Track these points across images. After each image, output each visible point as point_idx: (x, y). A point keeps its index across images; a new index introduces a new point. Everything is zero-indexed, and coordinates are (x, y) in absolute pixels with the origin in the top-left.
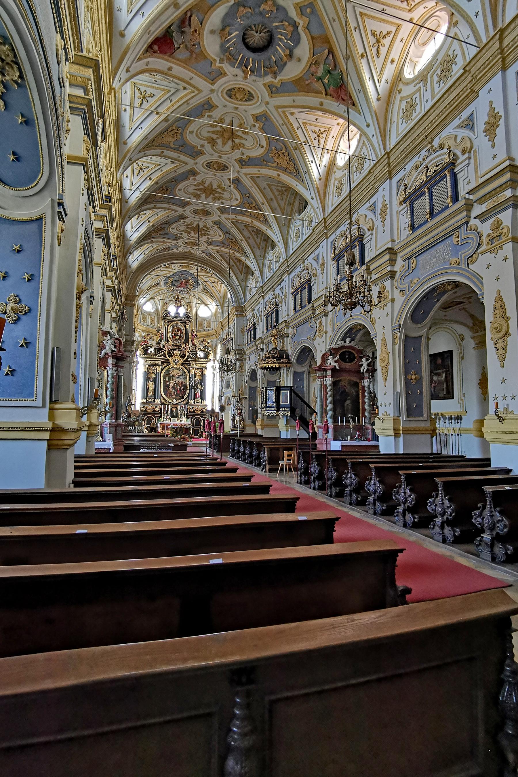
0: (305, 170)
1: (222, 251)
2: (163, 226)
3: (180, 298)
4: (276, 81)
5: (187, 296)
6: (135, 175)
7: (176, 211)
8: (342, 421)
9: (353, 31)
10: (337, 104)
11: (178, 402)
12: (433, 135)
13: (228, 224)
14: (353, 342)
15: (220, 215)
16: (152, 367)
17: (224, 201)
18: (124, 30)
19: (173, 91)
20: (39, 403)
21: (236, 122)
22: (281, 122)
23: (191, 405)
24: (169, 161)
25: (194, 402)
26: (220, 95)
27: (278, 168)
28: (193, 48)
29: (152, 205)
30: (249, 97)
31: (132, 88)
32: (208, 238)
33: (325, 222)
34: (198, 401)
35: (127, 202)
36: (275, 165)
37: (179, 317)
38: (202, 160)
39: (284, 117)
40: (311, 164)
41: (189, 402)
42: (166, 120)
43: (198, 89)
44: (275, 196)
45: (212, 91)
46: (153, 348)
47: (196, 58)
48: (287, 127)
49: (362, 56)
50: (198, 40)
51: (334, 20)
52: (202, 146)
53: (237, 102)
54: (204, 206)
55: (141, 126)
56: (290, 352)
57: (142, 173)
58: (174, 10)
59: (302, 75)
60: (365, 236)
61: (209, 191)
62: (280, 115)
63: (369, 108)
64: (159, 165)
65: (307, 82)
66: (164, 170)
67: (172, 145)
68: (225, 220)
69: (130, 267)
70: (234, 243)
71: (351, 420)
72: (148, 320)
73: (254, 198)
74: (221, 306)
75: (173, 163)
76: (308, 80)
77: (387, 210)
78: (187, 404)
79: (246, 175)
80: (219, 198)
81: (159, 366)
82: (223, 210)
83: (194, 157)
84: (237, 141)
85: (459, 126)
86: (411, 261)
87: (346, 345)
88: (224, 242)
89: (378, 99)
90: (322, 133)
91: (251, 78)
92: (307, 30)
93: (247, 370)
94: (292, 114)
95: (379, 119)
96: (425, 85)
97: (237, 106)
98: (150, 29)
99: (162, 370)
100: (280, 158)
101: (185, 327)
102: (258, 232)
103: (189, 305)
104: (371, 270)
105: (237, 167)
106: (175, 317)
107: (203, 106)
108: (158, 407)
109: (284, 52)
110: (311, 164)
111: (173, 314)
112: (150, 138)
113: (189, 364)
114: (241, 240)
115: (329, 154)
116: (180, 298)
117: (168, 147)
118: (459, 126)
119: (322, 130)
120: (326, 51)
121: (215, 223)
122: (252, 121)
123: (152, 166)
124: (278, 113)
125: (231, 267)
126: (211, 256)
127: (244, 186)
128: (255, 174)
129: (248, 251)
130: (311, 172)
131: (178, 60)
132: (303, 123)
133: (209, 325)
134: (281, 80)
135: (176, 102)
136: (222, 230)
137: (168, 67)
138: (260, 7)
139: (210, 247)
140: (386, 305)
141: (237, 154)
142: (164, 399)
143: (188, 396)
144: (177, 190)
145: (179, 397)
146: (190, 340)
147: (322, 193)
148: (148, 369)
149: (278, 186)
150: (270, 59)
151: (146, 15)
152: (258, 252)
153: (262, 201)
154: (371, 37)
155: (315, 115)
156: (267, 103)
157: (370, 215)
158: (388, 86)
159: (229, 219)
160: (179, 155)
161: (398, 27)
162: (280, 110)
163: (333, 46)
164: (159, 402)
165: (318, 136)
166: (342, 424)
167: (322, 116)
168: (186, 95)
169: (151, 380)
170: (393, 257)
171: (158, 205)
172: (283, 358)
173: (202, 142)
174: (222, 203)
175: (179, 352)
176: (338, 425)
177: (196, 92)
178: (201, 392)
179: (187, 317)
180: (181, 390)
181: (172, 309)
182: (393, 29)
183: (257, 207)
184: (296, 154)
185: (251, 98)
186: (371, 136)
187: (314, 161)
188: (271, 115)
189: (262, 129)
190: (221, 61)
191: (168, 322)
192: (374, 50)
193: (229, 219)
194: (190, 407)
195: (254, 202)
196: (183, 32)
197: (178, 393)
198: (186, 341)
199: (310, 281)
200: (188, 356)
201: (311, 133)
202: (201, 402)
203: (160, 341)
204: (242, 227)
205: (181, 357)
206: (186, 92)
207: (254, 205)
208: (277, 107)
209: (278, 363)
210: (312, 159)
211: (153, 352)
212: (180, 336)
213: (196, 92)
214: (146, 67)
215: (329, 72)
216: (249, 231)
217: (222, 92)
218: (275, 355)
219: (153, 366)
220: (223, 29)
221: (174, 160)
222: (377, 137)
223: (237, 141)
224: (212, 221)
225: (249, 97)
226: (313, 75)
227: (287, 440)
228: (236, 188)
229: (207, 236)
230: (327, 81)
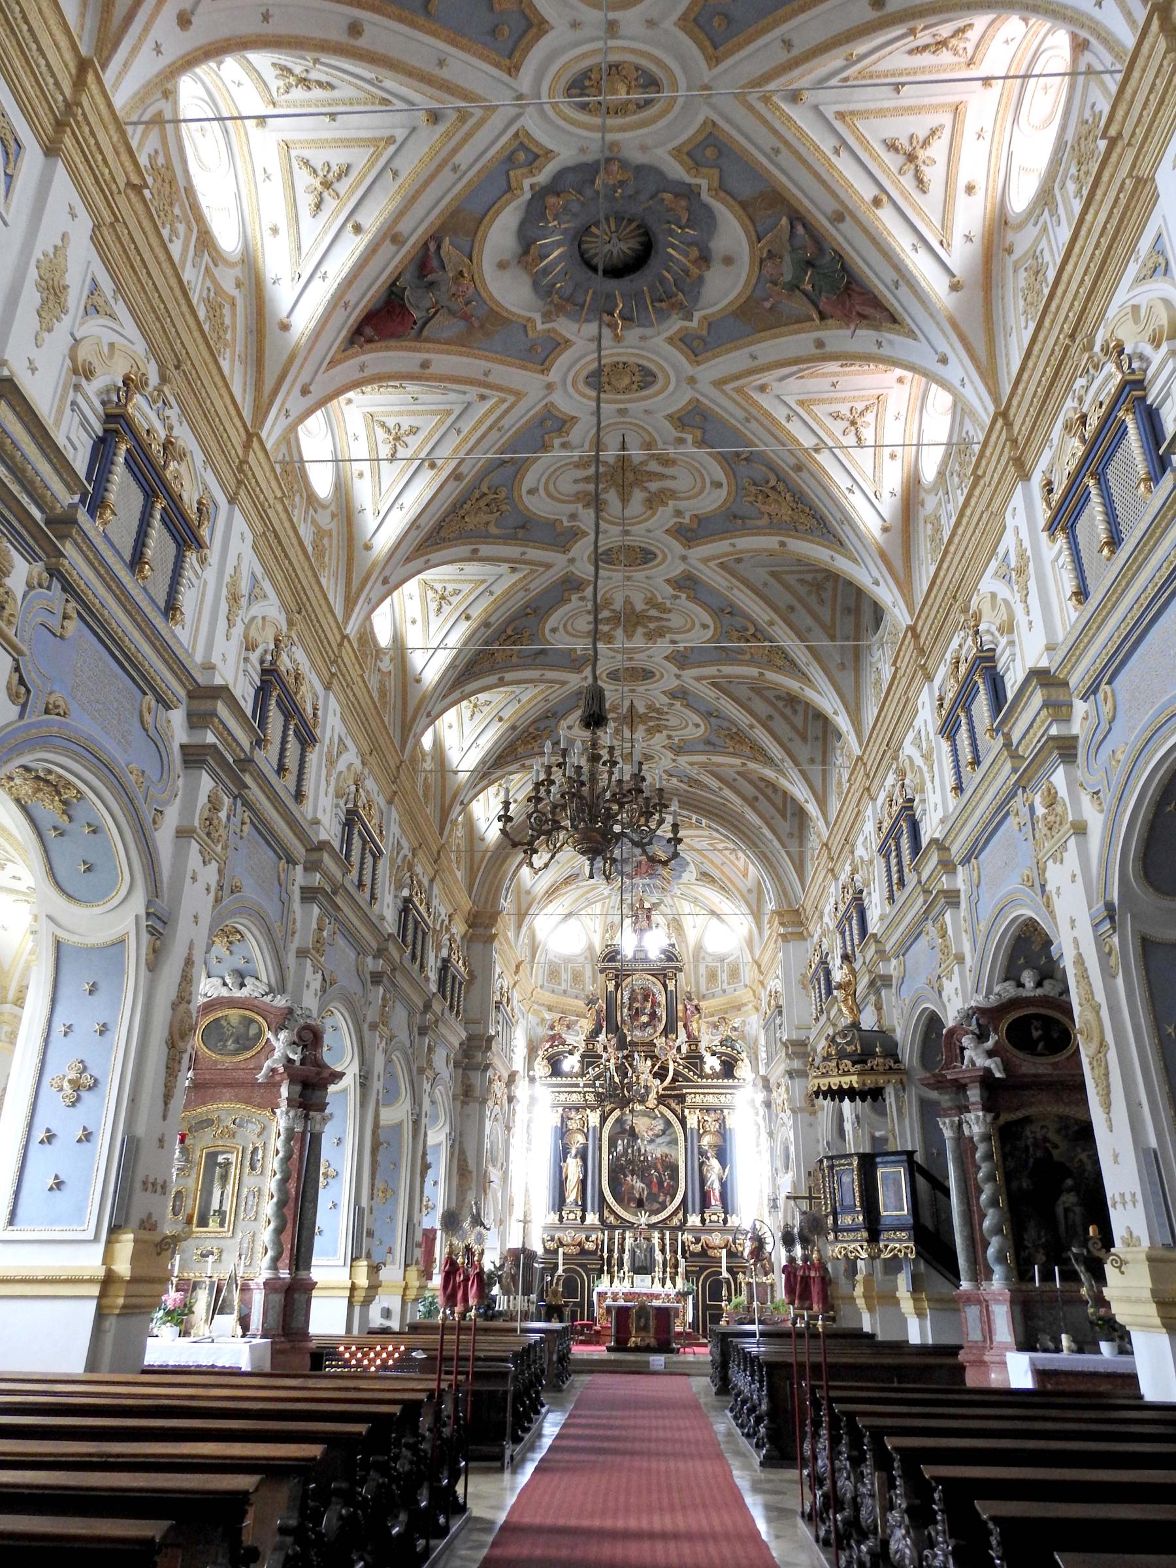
0: (839, 516)
1: (714, 764)
2: (542, 725)
3: (647, 905)
4: (694, 324)
5: (668, 900)
6: (432, 615)
7: (563, 683)
8: (1047, 1276)
9: (834, 158)
10: (849, 332)
11: (655, 1219)
12: (1086, 329)
13: (709, 693)
14: (1047, 983)
15: (684, 552)
16: (573, 1114)
17: (677, 637)
18: (288, 316)
19: (457, 411)
20: (90, 1235)
21: (633, 440)
22: (741, 414)
23: (691, 1230)
24: (504, 568)
25: (703, 1221)
26: (570, 389)
27: (775, 526)
28: (468, 309)
29: (493, 679)
30: (646, 378)
31: (367, 425)
32: (669, 737)
33: (916, 636)
34: (714, 1218)
35: (418, 681)
36: (765, 521)
37: (645, 960)
38: (582, 549)
39: (743, 403)
40: (850, 496)
41: (685, 1220)
42: (456, 476)
43: (510, 391)
44: (800, 600)
45: (550, 387)
46: (577, 1056)
47: (482, 327)
48: (761, 424)
49: (877, 202)
50: (472, 289)
51: (777, 151)
52: (573, 517)
53: (619, 397)
54: (631, 659)
55: (400, 502)
56: (898, 1035)
57: (446, 608)
58: (394, 248)
59: (748, 293)
60: (999, 651)
61: (631, 620)
62: (731, 398)
63: (931, 315)
64: (484, 581)
65: (767, 305)
66: (499, 590)
67: (493, 530)
68: (695, 684)
69: (483, 840)
70: (737, 738)
71: (1080, 1269)
72: (564, 976)
73: (747, 617)
74: (752, 913)
75: (514, 570)
76: (767, 299)
77: (1027, 565)
78: (682, 1227)
79: (705, 561)
80: (660, 633)
81: (593, 1109)
82: (681, 659)
83: (544, 365)
84: (654, 486)
85: (1140, 279)
86: (1101, 695)
87: (1025, 993)
88: (714, 739)
89: (955, 287)
90: (862, 414)
91: (633, 335)
92: (722, 194)
93: (967, 948)
94: (763, 388)
95: (971, 337)
96: (1054, 213)
97: (622, 406)
98: (346, 298)
99: (603, 1119)
100: (770, 500)
101: (665, 986)
102: (792, 700)
103: (676, 925)
104: (1015, 742)
105: (677, 547)
106: (635, 960)
107: (542, 423)
108: (593, 1237)
109: (686, 255)
110: (850, 496)
111: (628, 951)
112: (427, 524)
113: (681, 1099)
114: (751, 727)
115: (899, 461)
116: (647, 905)
117: (486, 538)
118: (1140, 279)
119: (860, 406)
120: (784, 221)
121: (673, 695)
122: (672, 432)
123: (466, 588)
124: (726, 394)
125: (752, 802)
126: (693, 782)
127: (712, 591)
128: (727, 555)
129: (775, 751)
130: (854, 515)
131: (439, 342)
132: (801, 403)
133: (734, 974)
134: (705, 318)
135: (470, 433)
136: (696, 711)
137: (419, 362)
138: (593, 182)
139: (683, 760)
140: (1064, 846)
141: (664, 516)
142: (612, 1212)
143: (684, 1201)
144: (547, 632)
145: (656, 1206)
146: (680, 1024)
147: (898, 564)
148: (564, 1119)
149: (799, 572)
150: (662, 281)
151: (330, 275)
152: (804, 751)
153: (767, 618)
154: (888, 158)
155: (825, 375)
156: (692, 380)
157: (1003, 591)
158: (976, 247)
159: (705, 678)
160: (522, 549)
161: (957, 110)
162: (728, 388)
163: (796, 204)
164: (597, 1222)
165: (853, 423)
166: (1048, 1286)
167: (845, 374)
168: (491, 411)
169: (573, 1151)
170: (1058, 695)
171: (509, 676)
172: (873, 1055)
173: (570, 509)
174: (673, 642)
175: (649, 1063)
176: (1056, 1291)
177: (512, 399)
178: (723, 1185)
179: (669, 959)
180: (660, 1183)
181: (628, 944)
182: (946, 119)
183: (759, 634)
184: (800, 480)
185: (649, 379)
186: (957, 384)
187: (855, 488)
188: (713, 406)
189: (701, 443)
190: (547, 317)
191: (617, 976)
192: (908, 181)
193: (705, 678)
194: (688, 1237)
195: (750, 625)
196: (431, 285)
197: (655, 1190)
198: (670, 1030)
199: (911, 808)
200: (676, 1073)
201: (829, 422)
202: (725, 1221)
203: (595, 1033)
204: (743, 692)
205: (655, 1075)
206: (488, 404)
207: (752, 631)
208: (719, 384)
209: (859, 1074)
210: (849, 483)
211: (577, 1069)
212: (653, 1015)
213: (512, 399)
214: (362, 375)
215: (810, 264)
216: (767, 700)
217: (574, 384)
218: (849, 1049)
219: (577, 1109)
220: (526, 252)
221: (515, 564)
222: (972, 382)
223: (654, 486)
224: (664, 692)
225: (646, 378)
226: (775, 283)
227: (922, 1350)
228: (694, 599)
229: (665, 733)
230: (809, 288)
